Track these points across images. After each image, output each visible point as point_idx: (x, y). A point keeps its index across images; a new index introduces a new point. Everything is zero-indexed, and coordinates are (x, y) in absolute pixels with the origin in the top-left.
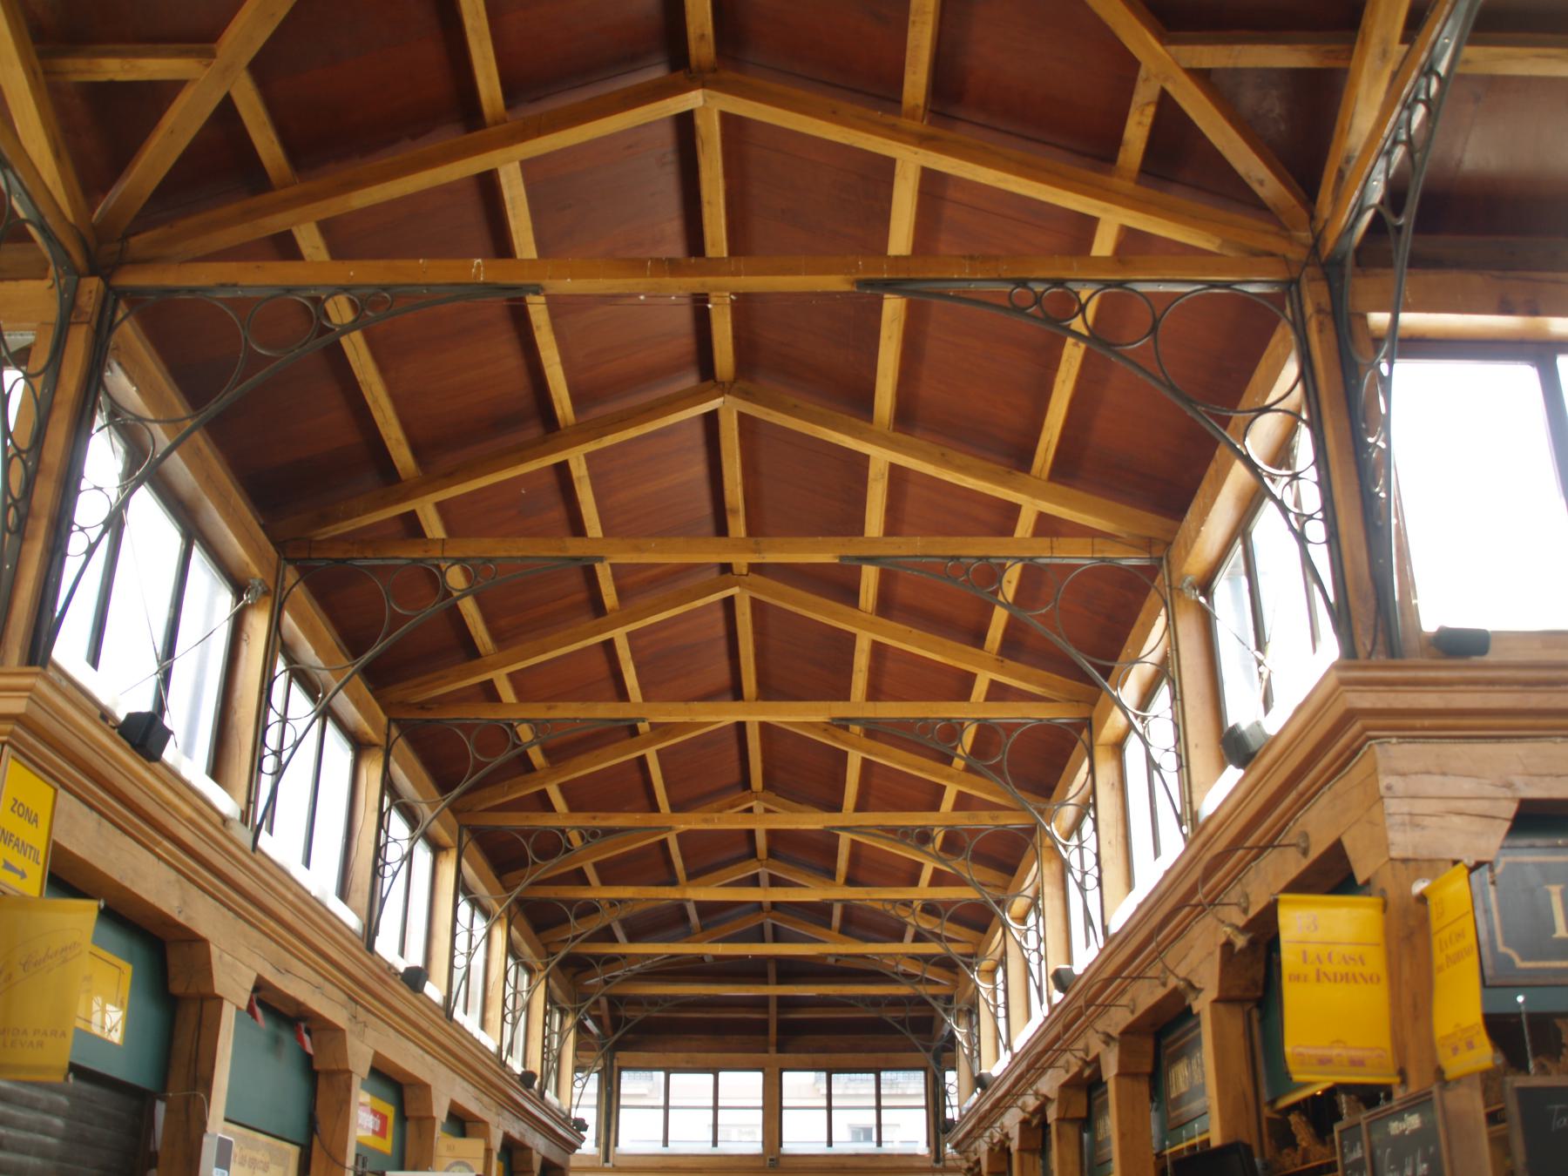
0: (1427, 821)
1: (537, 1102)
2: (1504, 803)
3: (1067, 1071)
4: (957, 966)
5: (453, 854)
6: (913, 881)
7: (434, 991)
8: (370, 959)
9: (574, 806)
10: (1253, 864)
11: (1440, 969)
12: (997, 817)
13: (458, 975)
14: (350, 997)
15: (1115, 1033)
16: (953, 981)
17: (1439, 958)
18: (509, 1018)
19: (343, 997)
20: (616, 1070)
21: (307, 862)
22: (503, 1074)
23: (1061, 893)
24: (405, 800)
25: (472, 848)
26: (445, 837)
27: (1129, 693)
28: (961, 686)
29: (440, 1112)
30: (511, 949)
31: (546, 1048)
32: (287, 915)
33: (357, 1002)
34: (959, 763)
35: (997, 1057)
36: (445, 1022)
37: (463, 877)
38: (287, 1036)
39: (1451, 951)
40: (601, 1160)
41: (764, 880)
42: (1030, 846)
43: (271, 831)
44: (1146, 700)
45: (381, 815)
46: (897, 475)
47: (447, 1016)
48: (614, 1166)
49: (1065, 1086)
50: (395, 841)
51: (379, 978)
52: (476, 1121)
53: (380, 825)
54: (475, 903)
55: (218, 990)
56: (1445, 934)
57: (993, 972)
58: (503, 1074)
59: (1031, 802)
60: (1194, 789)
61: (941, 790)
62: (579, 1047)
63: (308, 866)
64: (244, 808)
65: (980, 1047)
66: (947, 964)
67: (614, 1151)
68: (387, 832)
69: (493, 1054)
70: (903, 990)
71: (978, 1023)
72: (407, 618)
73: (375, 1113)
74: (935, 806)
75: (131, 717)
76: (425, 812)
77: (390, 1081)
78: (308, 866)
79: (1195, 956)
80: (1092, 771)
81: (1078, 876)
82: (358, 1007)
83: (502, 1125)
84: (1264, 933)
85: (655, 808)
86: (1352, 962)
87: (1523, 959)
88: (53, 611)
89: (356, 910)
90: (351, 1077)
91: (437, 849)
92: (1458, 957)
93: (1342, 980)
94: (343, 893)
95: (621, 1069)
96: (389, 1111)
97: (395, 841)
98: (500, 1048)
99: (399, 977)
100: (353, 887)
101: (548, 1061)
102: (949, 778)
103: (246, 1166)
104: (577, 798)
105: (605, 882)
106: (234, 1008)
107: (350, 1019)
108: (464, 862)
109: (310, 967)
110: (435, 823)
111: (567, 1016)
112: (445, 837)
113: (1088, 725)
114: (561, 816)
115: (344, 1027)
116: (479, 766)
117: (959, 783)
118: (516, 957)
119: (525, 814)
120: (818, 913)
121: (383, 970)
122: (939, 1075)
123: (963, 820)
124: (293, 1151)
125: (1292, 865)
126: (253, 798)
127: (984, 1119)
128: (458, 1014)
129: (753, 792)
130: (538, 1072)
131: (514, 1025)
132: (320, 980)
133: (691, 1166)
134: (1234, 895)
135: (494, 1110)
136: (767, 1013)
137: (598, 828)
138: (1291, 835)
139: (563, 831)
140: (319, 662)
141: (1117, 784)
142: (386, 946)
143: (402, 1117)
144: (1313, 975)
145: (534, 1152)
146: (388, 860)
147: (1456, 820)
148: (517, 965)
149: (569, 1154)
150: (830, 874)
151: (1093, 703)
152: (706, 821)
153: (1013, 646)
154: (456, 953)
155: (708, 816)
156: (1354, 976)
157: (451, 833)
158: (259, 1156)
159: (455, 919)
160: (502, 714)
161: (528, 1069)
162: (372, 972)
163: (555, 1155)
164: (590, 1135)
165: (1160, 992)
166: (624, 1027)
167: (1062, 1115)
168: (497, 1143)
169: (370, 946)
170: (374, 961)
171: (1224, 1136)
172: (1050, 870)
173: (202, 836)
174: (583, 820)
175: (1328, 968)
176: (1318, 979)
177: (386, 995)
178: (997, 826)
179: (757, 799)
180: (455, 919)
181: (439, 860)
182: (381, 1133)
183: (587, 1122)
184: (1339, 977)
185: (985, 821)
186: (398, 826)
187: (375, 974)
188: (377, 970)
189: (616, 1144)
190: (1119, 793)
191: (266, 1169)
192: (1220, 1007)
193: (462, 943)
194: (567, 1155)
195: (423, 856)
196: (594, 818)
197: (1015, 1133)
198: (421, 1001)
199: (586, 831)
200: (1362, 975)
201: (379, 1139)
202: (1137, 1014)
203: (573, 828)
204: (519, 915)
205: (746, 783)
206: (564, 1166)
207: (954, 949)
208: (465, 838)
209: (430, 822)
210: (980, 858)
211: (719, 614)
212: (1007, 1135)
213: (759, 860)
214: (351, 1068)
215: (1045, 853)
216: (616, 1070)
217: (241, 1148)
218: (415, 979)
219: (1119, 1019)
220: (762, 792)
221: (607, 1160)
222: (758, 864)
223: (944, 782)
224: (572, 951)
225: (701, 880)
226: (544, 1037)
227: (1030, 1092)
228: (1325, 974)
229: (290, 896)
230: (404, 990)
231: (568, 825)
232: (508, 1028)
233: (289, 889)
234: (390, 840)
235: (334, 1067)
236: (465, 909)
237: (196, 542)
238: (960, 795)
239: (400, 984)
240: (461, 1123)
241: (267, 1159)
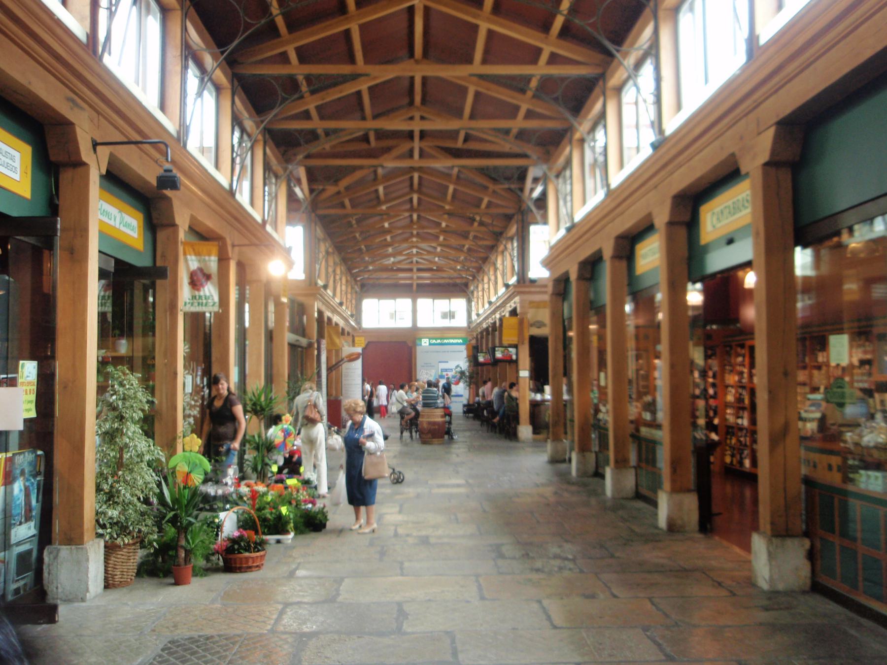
6: (534, 60)
12: (445, 316)
27: (630, 61)
28: (533, 55)
34: (529, 94)
35: (595, 192)
43: (110, 54)
44: (638, 65)
46: (491, 33)
64: (178, 128)
69: (84, 45)
72: (253, 25)
80: (656, 32)
82: (101, 118)
98: (231, 185)
104: (304, 56)
113: (602, 77)
116: (248, 26)
123: (556, 71)
128: (238, 196)
151: (609, 64)
153: (566, 32)
211: (405, 17)
215: (575, 143)
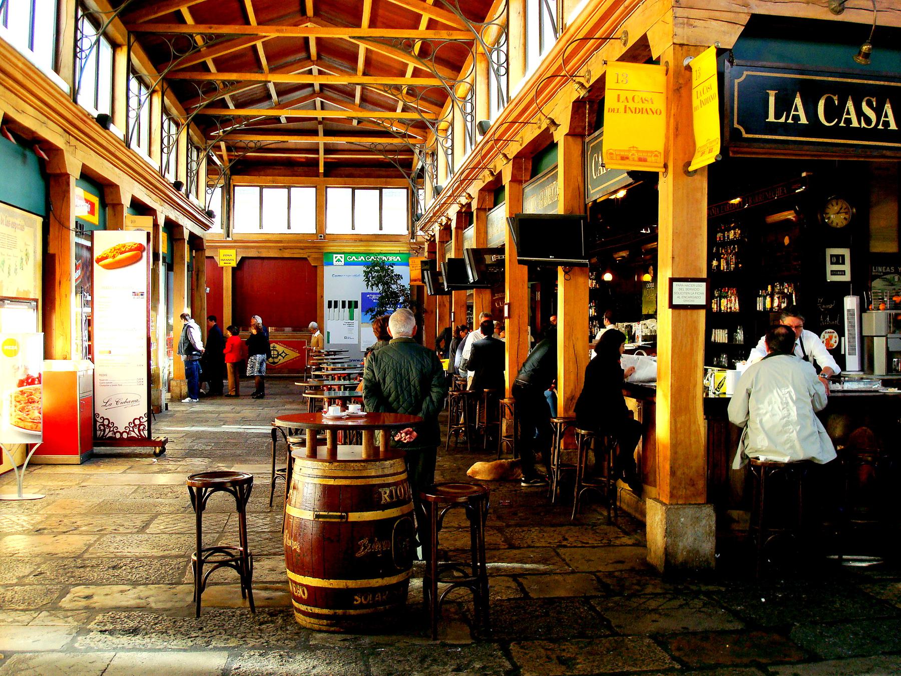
0: (697, 23)
2: (743, 15)
3: (484, 182)
4: (427, 127)
5: (125, 49)
7: (117, 129)
8: (75, 107)
9: (198, 20)
10: (595, 53)
11: (696, 109)
13: (132, 122)
14: (65, 130)
15: (511, 156)
16: (424, 136)
17: (696, 102)
18: (165, 150)
19: (60, 130)
21: (31, 47)
22: (163, 182)
23: (486, 81)
24: (91, 11)
25: (136, 46)
26: (120, 38)
29: (126, 201)
30: (165, 110)
31: (188, 170)
32: (19, 77)
33: (69, 134)
37: (132, 64)
38: (28, 153)
39: (703, 98)
40: (225, 235)
41: (315, 72)
42: (471, 53)
45: (77, 20)
49: (482, 191)
50: (86, 37)
51: (82, 119)
53: (76, 28)
54: (141, 80)
56: (700, 88)
57: (446, 130)
58: (163, 182)
59: (471, 25)
60: (565, 10)
61: (419, 16)
62: (209, 172)
63: (32, 49)
65: (437, 173)
66: (422, 126)
68: (82, 32)
70: (396, 141)
71: (437, 159)
73: (87, 201)
74: (416, 26)
76: (105, 19)
77: (89, 178)
78: (32, 49)
79: (558, 110)
81: (496, 67)
83: (164, 212)
84: (599, 87)
85: (247, 22)
86: (646, 102)
87: (738, 123)
89: (65, 80)
90: (69, 178)
91: (115, 46)
92: (707, 101)
93: (639, 112)
94: (56, 68)
96: (96, 200)
97: (86, 37)
99: (95, 120)
100: (62, 65)
101: (191, 177)
102: (424, 9)
103: (10, 227)
105: (220, 70)
107: (65, 143)
108: (132, 55)
112: (120, 38)
114: (216, 76)
115: (62, 148)
117: (431, 13)
118: (168, 114)
119: (168, 25)
120: (346, 93)
121: (84, 115)
122: (415, 191)
123: (431, 35)
124: (39, 220)
125: (616, 49)
127: (440, 210)
129: (307, 17)
130: (184, 182)
131: (169, 153)
132: (45, 118)
133: (274, 239)
134: (582, 72)
136: (318, 154)
137: (213, 34)
138: (619, 33)
139: (191, 36)
141: (522, 13)
142: (85, 100)
143: (103, 204)
144: (622, 110)
145: (184, 229)
146: (84, 49)
147: (714, 22)
148: (169, 119)
150: (355, 69)
152: (278, 31)
154: (130, 109)
155: (279, 28)
156: (646, 110)
157: (123, 36)
158: (17, 222)
159: (128, 89)
160: (183, 30)
161: (178, 180)
162: (77, 115)
163: (198, 231)
164: (217, 220)
165: (537, 132)
167: (479, 207)
168: (161, 222)
169: (75, 101)
170: (77, 109)
171: (565, 210)
172: (481, 67)
174: (203, 29)
175: (631, 105)
176: (625, 112)
177: (87, 130)
178: (451, 40)
179: (310, 21)
180: (128, 89)
182: (92, 212)
183: (215, 214)
184: (637, 111)
185: (444, 36)
186: (88, 28)
187: (79, 117)
188: (80, 115)
190: (523, 18)
191: (22, 229)
192: (569, 138)
193: (134, 102)
195: (106, 49)
196: (211, 28)
197: (454, 218)
198: (109, 135)
199: (206, 36)
200: (651, 109)
201: (91, 216)
202: (524, 145)
203: (198, 34)
204: (168, 89)
205: (303, 11)
206: (202, 237)
207: (427, 116)
208: (132, 40)
209: (107, 26)
210: (440, 60)
212: (449, 219)
213: (312, 61)
214: (68, 172)
217: (6, 217)
218: (104, 121)
219: (514, 149)
220: (314, 17)
222: (311, 63)
223: (421, 12)
224: (200, 113)
225: (277, 71)
226: (187, 164)
227: (464, 194)
228: (629, 108)
229: (20, 65)
230: (97, 127)
231: (195, 32)
232: (165, 156)
233: (19, 60)
234: (84, 36)
235: (58, 172)
236: (134, 83)
238: (431, 21)
239: (95, 124)
240: (140, 208)
241: (22, 223)
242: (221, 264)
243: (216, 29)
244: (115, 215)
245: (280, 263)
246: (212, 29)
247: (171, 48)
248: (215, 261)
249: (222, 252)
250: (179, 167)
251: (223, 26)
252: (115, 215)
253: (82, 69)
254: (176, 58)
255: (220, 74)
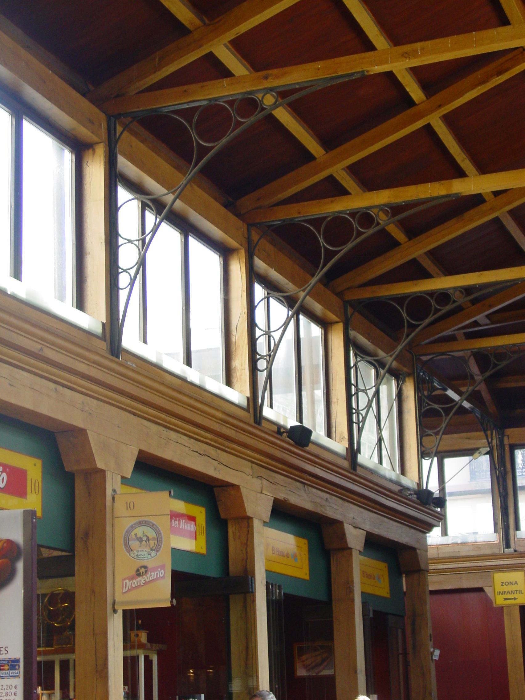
1: (252, 430)
5: (101, 151)
20: (507, 449)
36: (111, 361)
47: (255, 422)
48: (515, 551)
52: (226, 486)
55: (249, 513)
63: (145, 342)
67: (515, 535)
75: (291, 427)
88: (118, 319)
95: (513, 448)
106: (358, 551)
109: (113, 405)
110: (308, 298)
111: (404, 381)
115: (81, 425)
116: (437, 311)
126: (421, 477)
135: (248, 471)
140: (164, 191)
149: (425, 533)
166: (433, 315)
173: (128, 381)
181: (85, 166)
189: (517, 528)
194: (421, 534)
196: (266, 78)
216: (507, 449)
221: (508, 546)
237: (119, 183)
242: (499, 601)
243: (277, 77)
244: (89, 495)
245: (241, 263)
246: (270, 79)
247: (321, 240)
248: (486, 596)
249: (499, 577)
250: (333, 399)
251: (290, 68)
252: (89, 495)
253: (360, 430)
254: (412, 327)
255: (329, 174)
